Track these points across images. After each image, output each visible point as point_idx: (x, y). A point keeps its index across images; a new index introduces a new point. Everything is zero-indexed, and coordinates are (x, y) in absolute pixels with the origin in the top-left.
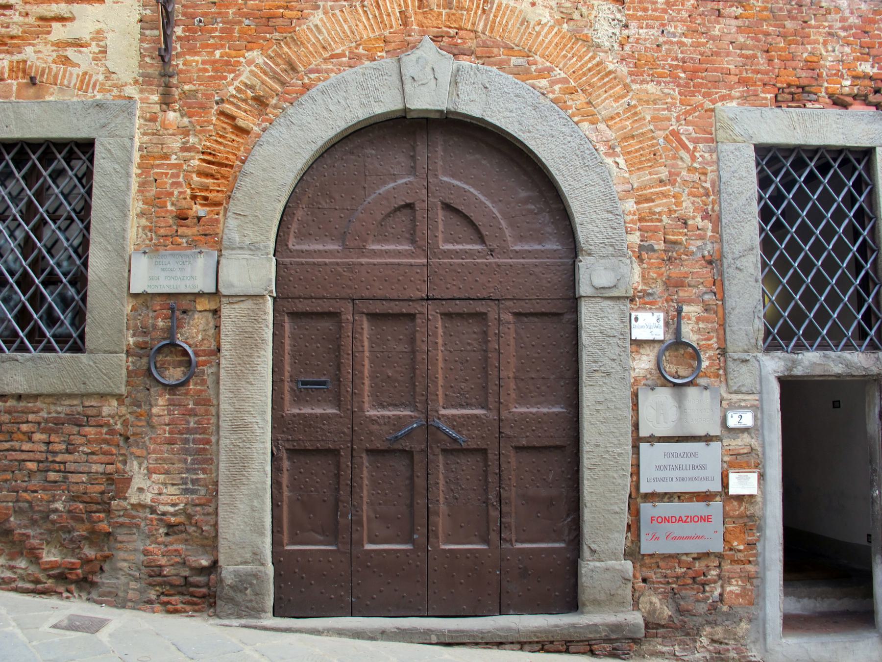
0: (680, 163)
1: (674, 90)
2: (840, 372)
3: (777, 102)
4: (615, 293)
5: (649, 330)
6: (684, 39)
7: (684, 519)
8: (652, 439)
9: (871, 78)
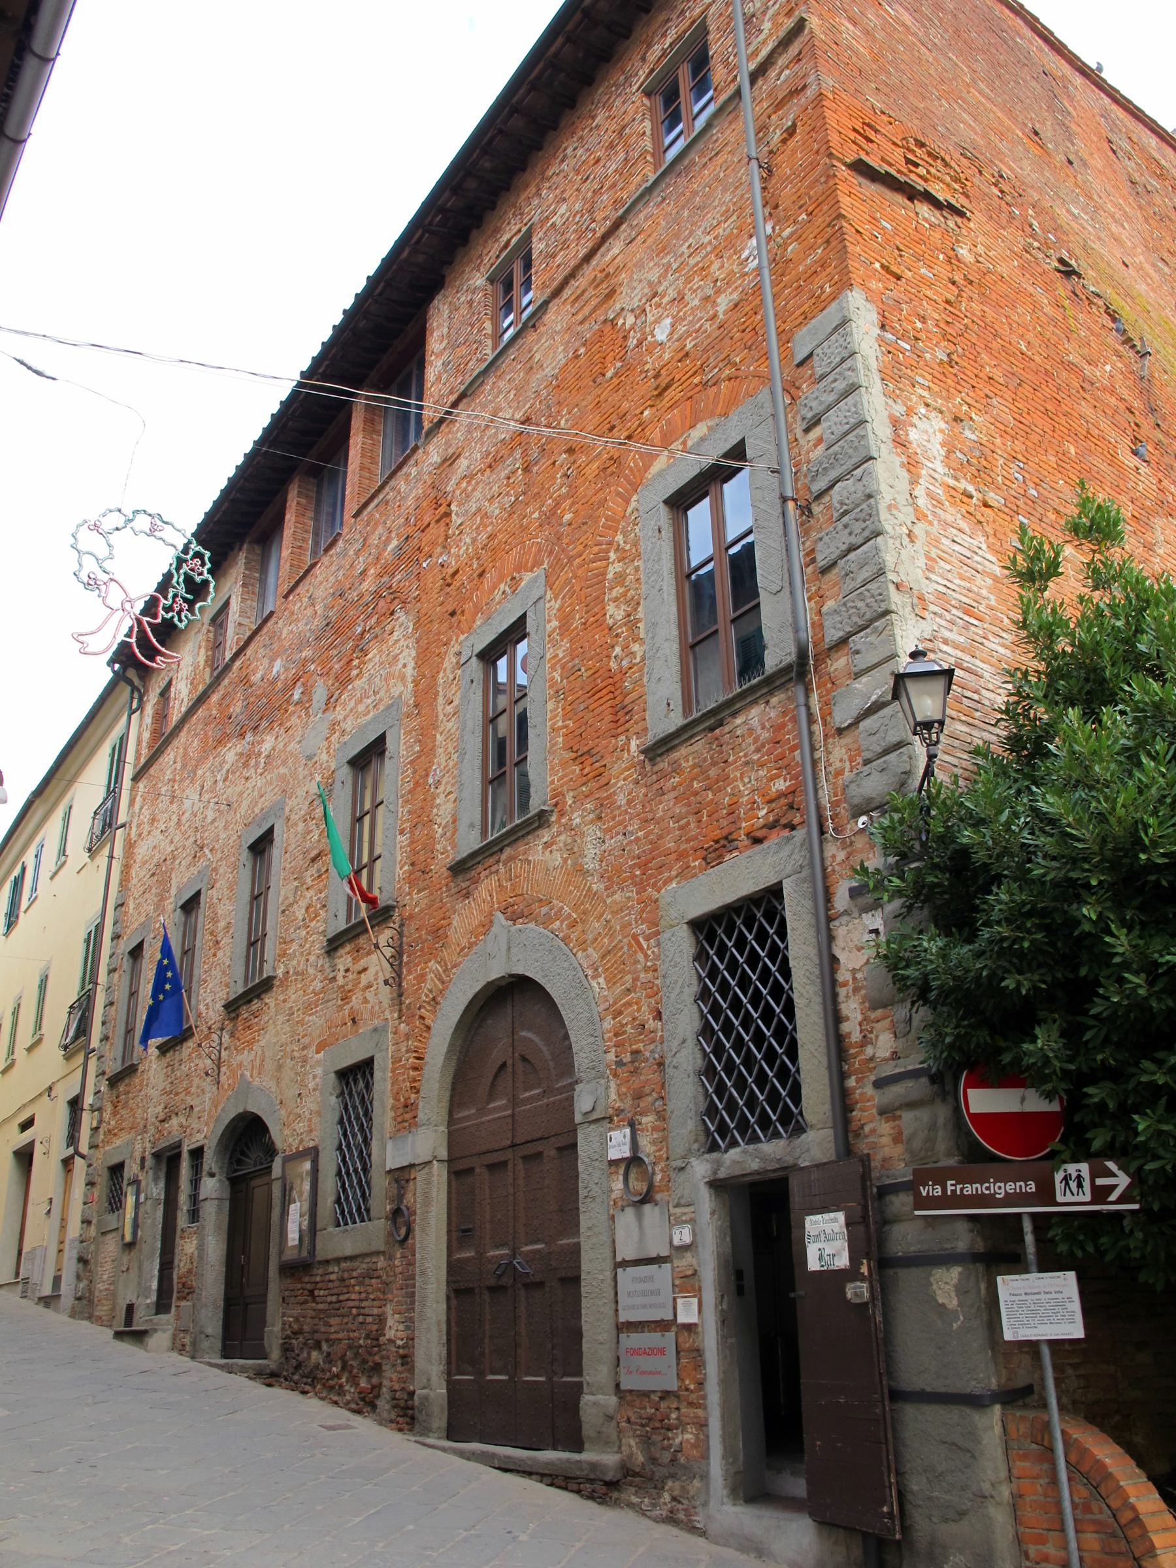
3: (708, 863)
4: (595, 1116)
8: (625, 1264)
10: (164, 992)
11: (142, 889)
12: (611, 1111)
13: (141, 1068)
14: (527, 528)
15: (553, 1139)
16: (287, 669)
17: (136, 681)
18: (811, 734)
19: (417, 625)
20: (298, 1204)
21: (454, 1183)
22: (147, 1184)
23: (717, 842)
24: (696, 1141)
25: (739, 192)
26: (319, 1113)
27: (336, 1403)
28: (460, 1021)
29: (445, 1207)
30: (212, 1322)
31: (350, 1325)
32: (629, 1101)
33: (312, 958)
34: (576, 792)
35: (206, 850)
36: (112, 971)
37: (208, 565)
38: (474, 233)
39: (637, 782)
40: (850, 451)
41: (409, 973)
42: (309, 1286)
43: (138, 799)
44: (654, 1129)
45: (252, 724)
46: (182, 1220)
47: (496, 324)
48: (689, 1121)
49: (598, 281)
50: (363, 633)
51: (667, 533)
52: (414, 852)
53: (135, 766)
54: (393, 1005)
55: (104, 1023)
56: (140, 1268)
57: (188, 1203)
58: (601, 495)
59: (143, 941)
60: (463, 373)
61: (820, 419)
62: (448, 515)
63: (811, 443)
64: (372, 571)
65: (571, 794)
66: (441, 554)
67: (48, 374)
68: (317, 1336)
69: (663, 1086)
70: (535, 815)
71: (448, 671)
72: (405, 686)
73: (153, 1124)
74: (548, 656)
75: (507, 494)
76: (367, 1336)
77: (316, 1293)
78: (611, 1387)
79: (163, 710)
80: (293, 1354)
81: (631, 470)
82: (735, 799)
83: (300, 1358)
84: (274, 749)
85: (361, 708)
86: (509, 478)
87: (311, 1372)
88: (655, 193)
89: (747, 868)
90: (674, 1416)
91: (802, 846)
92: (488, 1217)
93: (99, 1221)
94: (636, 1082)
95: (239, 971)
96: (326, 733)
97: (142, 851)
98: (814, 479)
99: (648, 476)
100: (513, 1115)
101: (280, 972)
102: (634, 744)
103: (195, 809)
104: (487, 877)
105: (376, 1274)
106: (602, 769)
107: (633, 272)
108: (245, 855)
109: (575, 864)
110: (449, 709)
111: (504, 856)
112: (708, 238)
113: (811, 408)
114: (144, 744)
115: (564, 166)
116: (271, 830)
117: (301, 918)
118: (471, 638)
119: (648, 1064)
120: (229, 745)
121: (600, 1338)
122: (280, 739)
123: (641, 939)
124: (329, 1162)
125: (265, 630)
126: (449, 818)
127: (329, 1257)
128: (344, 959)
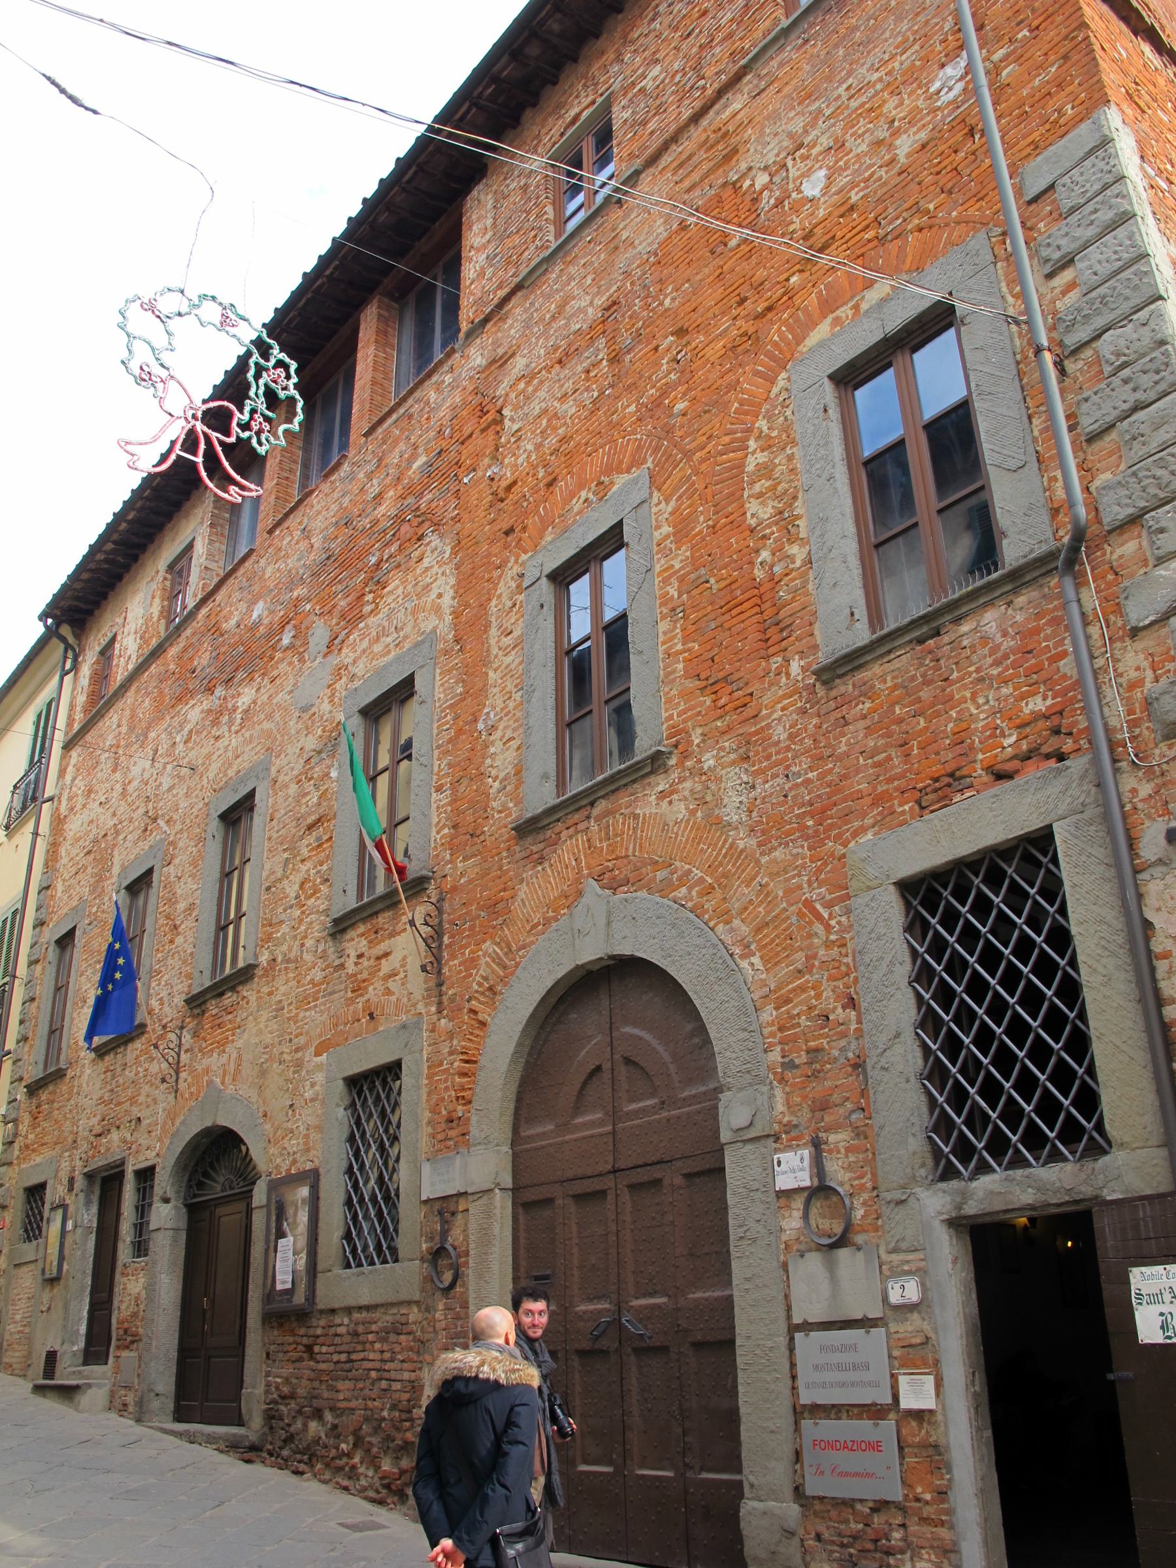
0: (816, 941)
1: (802, 847)
2: (1030, 1202)
4: (752, 1133)
5: (793, 1175)
6: (810, 775)
7: (850, 1444)
8: (807, 1327)
9: (1046, 717)
10: (114, 981)
11: (74, 870)
12: (776, 1127)
13: (70, 1074)
14: (619, 424)
15: (679, 1164)
16: (271, 612)
17: (71, 639)
18: (1088, 637)
19: (457, 547)
20: (291, 1239)
21: (521, 1218)
22: (77, 1210)
23: (936, 780)
24: (923, 1165)
25: (922, 18)
26: (319, 1128)
27: (346, 1489)
28: (532, 1015)
29: (510, 1247)
30: (164, 1380)
31: (366, 1391)
32: (806, 1113)
33: (309, 943)
34: (706, 729)
35: (161, 822)
36: (32, 963)
37: (295, 379)
38: (528, 113)
39: (803, 712)
40: (1127, 292)
41: (453, 957)
42: (305, 1341)
43: (70, 769)
44: (849, 1150)
45: (225, 677)
46: (124, 1252)
47: (559, 208)
48: (911, 1140)
49: (711, 142)
50: (378, 565)
51: (834, 413)
52: (457, 812)
53: (66, 733)
54: (429, 996)
55: (22, 1022)
56: (66, 1308)
57: (132, 1231)
58: (731, 377)
59: (74, 928)
60: (517, 264)
61: (1072, 261)
62: (499, 421)
63: (1057, 291)
64: (391, 493)
65: (699, 731)
66: (489, 466)
67: (86, 105)
68: (316, 1403)
69: (863, 1093)
70: (647, 758)
71: (504, 598)
72: (441, 618)
73: (86, 1138)
74: (658, 568)
75: (587, 389)
76: (394, 1407)
77: (316, 1349)
78: (788, 1492)
79: (103, 670)
80: (281, 1424)
81: (776, 344)
82: (964, 725)
83: (292, 1429)
84: (254, 702)
85: (377, 648)
86: (588, 372)
87: (308, 1448)
88: (793, 36)
89: (991, 810)
90: (897, 1535)
91: (1082, 778)
92: (576, 1262)
93: (11, 1250)
94: (816, 1089)
95: (205, 959)
96: (328, 679)
97: (74, 826)
98: (1068, 329)
99: (803, 348)
100: (614, 1133)
101: (264, 959)
102: (795, 667)
103: (146, 776)
104: (571, 837)
105: (405, 1329)
106: (748, 699)
107: (763, 127)
108: (215, 825)
109: (707, 817)
110: (507, 641)
111: (596, 811)
112: (876, 76)
113: (1059, 248)
114: (79, 708)
115: (656, 25)
116: (252, 794)
117: (293, 895)
118: (540, 556)
119: (838, 1065)
120: (192, 702)
121: (770, 1425)
122: (263, 691)
123: (818, 907)
124: (334, 1190)
125: (242, 571)
126: (510, 769)
127: (336, 1305)
128: (356, 942)
